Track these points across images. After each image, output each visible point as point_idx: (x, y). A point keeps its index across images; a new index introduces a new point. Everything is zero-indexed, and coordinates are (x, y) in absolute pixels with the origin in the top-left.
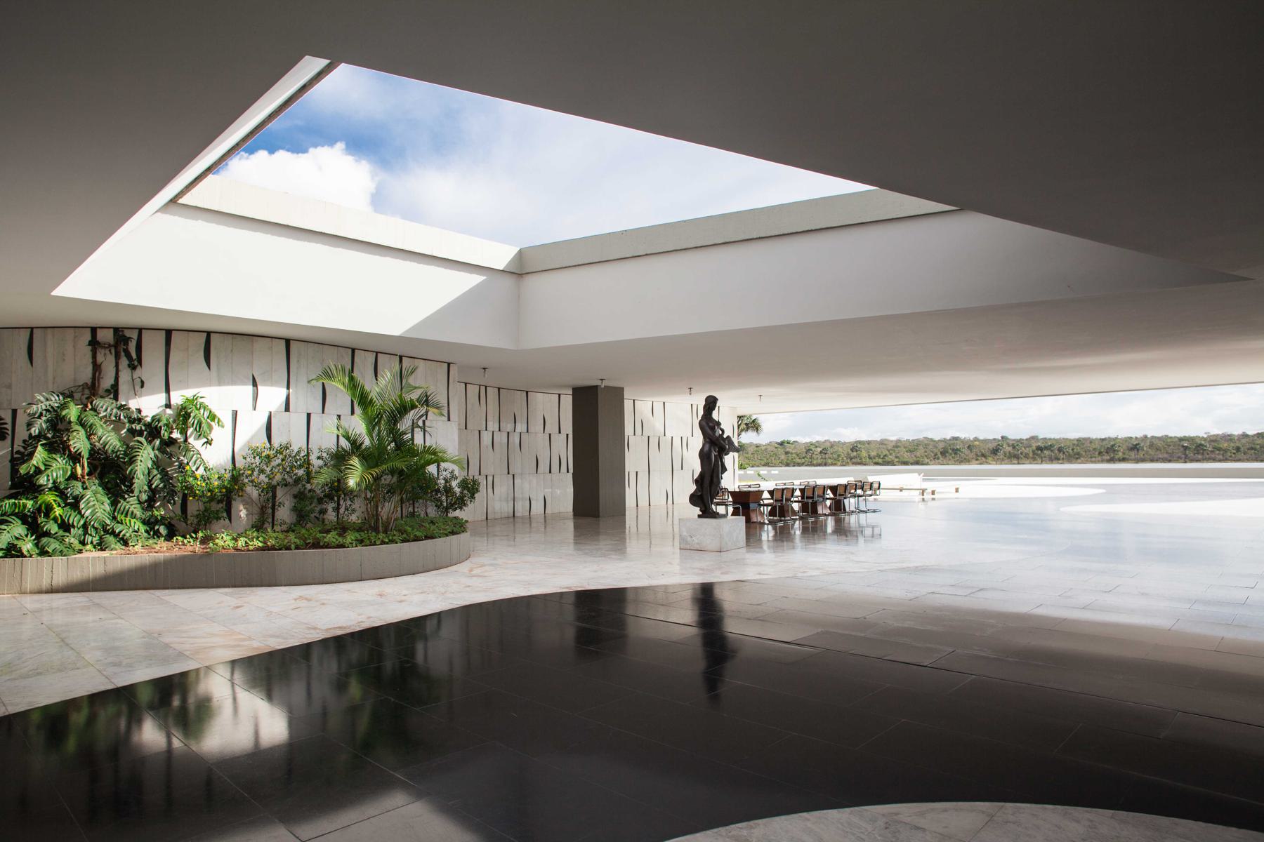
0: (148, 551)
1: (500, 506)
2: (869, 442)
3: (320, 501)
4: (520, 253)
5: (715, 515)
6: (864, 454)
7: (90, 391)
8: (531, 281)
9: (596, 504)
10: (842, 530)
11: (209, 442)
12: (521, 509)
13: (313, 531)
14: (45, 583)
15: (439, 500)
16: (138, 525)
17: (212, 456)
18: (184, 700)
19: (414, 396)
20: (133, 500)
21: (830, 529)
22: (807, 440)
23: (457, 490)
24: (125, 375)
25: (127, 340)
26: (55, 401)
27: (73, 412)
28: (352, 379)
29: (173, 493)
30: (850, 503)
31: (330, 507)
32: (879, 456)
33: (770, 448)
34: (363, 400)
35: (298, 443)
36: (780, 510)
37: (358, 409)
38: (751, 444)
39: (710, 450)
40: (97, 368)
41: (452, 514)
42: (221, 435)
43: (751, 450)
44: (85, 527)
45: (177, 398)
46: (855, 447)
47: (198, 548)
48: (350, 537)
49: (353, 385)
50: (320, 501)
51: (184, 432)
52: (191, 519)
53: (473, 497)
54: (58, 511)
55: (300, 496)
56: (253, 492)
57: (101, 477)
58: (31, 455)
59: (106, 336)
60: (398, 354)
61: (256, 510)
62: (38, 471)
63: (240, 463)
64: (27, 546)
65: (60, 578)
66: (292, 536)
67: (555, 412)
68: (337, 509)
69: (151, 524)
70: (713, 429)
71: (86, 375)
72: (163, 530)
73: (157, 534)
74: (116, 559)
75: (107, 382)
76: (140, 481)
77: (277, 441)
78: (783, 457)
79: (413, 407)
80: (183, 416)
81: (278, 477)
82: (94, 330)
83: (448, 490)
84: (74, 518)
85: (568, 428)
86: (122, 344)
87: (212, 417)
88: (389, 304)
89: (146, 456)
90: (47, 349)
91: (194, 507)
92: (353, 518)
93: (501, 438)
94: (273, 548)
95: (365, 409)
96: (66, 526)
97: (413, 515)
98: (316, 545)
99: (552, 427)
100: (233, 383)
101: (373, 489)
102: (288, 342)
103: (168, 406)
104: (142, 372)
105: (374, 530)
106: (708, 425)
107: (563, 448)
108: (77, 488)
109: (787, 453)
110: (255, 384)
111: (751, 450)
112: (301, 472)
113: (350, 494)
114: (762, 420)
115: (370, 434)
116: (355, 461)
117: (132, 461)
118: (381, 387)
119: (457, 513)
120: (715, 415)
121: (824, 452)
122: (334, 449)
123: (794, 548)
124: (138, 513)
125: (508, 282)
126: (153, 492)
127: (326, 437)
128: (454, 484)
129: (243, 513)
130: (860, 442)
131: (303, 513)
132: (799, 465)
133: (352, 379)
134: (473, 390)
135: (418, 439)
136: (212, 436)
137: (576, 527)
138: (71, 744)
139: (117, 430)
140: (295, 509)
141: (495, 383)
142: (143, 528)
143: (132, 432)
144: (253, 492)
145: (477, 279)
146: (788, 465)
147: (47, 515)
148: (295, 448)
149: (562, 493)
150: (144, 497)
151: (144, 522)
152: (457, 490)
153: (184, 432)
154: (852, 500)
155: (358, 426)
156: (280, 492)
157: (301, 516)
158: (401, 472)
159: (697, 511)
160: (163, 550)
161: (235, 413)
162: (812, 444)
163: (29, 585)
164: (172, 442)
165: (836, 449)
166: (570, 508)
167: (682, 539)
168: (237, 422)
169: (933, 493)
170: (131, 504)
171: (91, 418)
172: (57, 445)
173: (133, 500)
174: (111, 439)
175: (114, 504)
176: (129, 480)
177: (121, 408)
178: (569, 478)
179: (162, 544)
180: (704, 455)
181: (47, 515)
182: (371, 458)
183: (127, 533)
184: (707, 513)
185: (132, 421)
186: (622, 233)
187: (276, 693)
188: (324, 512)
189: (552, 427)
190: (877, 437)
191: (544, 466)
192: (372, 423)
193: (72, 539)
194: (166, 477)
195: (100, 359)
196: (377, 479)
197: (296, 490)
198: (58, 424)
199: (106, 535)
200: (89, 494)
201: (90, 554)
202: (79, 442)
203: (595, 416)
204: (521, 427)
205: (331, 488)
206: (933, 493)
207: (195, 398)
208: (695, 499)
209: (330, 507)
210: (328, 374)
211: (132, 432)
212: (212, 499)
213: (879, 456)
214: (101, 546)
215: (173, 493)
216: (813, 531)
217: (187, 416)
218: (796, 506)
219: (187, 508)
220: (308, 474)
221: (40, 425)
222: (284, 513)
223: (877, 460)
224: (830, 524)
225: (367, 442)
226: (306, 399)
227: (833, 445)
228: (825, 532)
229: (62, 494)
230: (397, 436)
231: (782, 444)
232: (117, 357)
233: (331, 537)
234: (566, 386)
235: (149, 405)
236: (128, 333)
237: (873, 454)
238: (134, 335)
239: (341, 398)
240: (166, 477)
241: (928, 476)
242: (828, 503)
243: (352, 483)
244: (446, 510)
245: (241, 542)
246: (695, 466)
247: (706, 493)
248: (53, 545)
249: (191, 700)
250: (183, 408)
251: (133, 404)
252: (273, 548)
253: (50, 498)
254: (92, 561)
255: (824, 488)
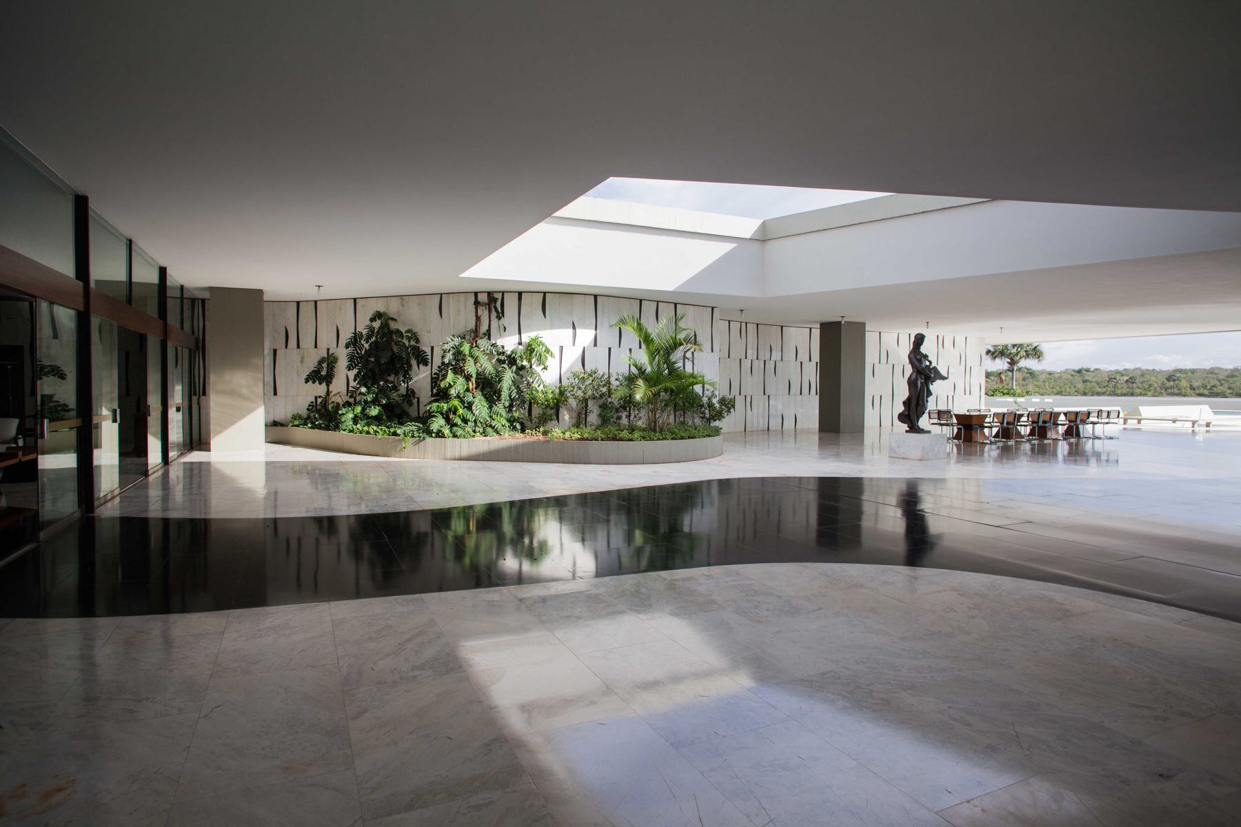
0: (511, 439)
1: (756, 419)
2: (1193, 371)
3: (617, 410)
4: (764, 223)
5: (920, 431)
6: (1184, 384)
7: (475, 335)
8: (770, 245)
9: (837, 420)
10: (1076, 453)
11: (545, 368)
12: (775, 424)
13: (613, 429)
14: (457, 455)
15: (703, 413)
16: (504, 422)
17: (547, 377)
18: (531, 542)
19: (681, 336)
20: (501, 406)
21: (1060, 456)
22: (1113, 368)
23: (717, 405)
24: (494, 322)
25: (495, 300)
26: (457, 341)
27: (466, 348)
28: (639, 324)
29: (523, 402)
30: (1086, 430)
31: (624, 415)
32: (1205, 387)
33: (1065, 376)
34: (647, 340)
35: (602, 370)
36: (1007, 430)
37: (643, 346)
38: (1043, 372)
39: (916, 380)
40: (478, 318)
41: (714, 424)
42: (552, 363)
43: (1042, 377)
44: (475, 422)
45: (526, 338)
46: (1171, 377)
47: (541, 438)
48: (637, 434)
49: (640, 328)
50: (617, 410)
51: (530, 361)
52: (535, 420)
53: (729, 411)
54: (461, 411)
55: (604, 407)
56: (573, 402)
57: (482, 390)
58: (445, 376)
59: (483, 298)
60: (675, 304)
61: (575, 415)
62: (450, 386)
63: (565, 383)
64: (446, 431)
65: (465, 453)
66: (599, 432)
67: (805, 343)
68: (628, 417)
69: (511, 421)
70: (920, 361)
71: (472, 325)
72: (518, 426)
73: (515, 428)
74: (492, 442)
75: (484, 328)
76: (505, 394)
77: (588, 368)
78: (1080, 386)
79: (681, 344)
80: (530, 350)
81: (590, 393)
82: (476, 294)
83: (710, 405)
84: (470, 416)
85: (816, 357)
86: (491, 302)
87: (547, 351)
88: (664, 269)
89: (509, 376)
90: (450, 306)
91: (536, 411)
92: (640, 423)
93: (758, 365)
94: (587, 439)
95: (648, 346)
96: (465, 421)
97: (683, 423)
98: (614, 439)
99: (803, 356)
100: (560, 327)
101: (652, 400)
102: (596, 297)
103: (520, 344)
104: (503, 321)
105: (654, 431)
106: (916, 356)
107: (812, 373)
108: (469, 398)
109: (1085, 381)
110: (574, 328)
111: (1042, 377)
112: (604, 390)
113: (637, 405)
114: (1044, 348)
115: (651, 364)
116: (640, 382)
117: (500, 381)
118: (659, 329)
119: (717, 423)
120: (923, 349)
121: (1131, 381)
122: (627, 374)
123: (983, 461)
124: (504, 414)
125: (756, 245)
126: (512, 400)
127: (621, 366)
128: (715, 401)
129: (567, 417)
130: (1180, 371)
131: (607, 414)
132: (1099, 394)
133: (639, 324)
134: (735, 327)
135: (689, 369)
136: (547, 363)
137: (820, 439)
138: (467, 561)
139: (490, 359)
140: (600, 415)
141: (755, 325)
142: (507, 424)
143: (499, 361)
144: (573, 402)
145: (730, 246)
146: (1085, 394)
147: (455, 413)
148: (600, 372)
149: (809, 411)
150: (507, 404)
151: (509, 421)
152: (717, 405)
153: (530, 361)
154: (1089, 427)
155: (643, 357)
156: (590, 403)
157: (604, 420)
158: (672, 390)
159: (905, 427)
160: (518, 438)
161: (562, 348)
162: (1117, 372)
163: (449, 455)
164: (523, 368)
165: (1148, 377)
166: (817, 426)
167: (892, 450)
168: (564, 353)
169: (1208, 425)
170: (500, 408)
171: (476, 352)
172: (459, 370)
173: (501, 406)
174: (488, 366)
175: (490, 407)
176: (498, 393)
177: (493, 345)
178: (815, 400)
179: (519, 435)
180: (912, 383)
181: (455, 413)
182: (651, 380)
183: (498, 426)
184: (914, 429)
185: (499, 354)
186: (842, 206)
187: (587, 536)
188: (619, 418)
189: (803, 356)
190: (1207, 365)
191: (795, 388)
192: (652, 356)
193: (469, 429)
194: (519, 391)
195: (480, 313)
196: (656, 395)
197: (601, 402)
198: (458, 354)
199: (488, 428)
200: (476, 400)
201: (479, 438)
202: (471, 368)
203: (838, 343)
204: (776, 355)
205: (625, 402)
206: (1208, 425)
207: (537, 338)
208: (902, 418)
209: (624, 415)
210: (623, 321)
211: (499, 361)
212: (547, 406)
213: (1205, 387)
214: (484, 434)
215: (523, 402)
216: (1042, 451)
217: (532, 351)
218: (1025, 431)
219: (534, 413)
220: (609, 390)
221: (449, 357)
222: (593, 418)
223: (1201, 391)
224: (1063, 448)
225: (649, 369)
226: (608, 337)
227: (1143, 373)
228: (1055, 454)
229: (462, 401)
230: (671, 366)
231: (1079, 371)
232: (490, 311)
233: (625, 434)
234: (815, 322)
235: (509, 343)
236: (496, 296)
237: (1195, 384)
238: (499, 296)
239: (631, 338)
240: (519, 391)
241: (1217, 411)
242: (1061, 429)
243: (638, 397)
244: (709, 420)
245: (567, 435)
246: (903, 393)
247: (912, 413)
248: (459, 432)
249: (535, 544)
250: (530, 345)
251: (499, 342)
252: (587, 439)
253: (456, 402)
254: (482, 443)
255: (1059, 414)
